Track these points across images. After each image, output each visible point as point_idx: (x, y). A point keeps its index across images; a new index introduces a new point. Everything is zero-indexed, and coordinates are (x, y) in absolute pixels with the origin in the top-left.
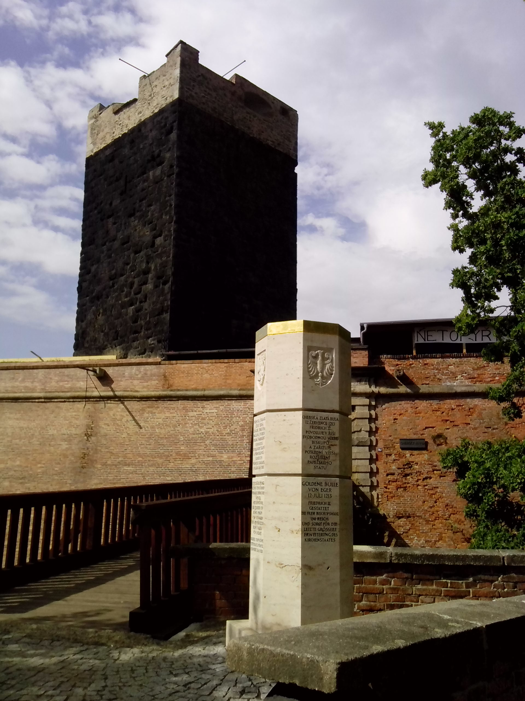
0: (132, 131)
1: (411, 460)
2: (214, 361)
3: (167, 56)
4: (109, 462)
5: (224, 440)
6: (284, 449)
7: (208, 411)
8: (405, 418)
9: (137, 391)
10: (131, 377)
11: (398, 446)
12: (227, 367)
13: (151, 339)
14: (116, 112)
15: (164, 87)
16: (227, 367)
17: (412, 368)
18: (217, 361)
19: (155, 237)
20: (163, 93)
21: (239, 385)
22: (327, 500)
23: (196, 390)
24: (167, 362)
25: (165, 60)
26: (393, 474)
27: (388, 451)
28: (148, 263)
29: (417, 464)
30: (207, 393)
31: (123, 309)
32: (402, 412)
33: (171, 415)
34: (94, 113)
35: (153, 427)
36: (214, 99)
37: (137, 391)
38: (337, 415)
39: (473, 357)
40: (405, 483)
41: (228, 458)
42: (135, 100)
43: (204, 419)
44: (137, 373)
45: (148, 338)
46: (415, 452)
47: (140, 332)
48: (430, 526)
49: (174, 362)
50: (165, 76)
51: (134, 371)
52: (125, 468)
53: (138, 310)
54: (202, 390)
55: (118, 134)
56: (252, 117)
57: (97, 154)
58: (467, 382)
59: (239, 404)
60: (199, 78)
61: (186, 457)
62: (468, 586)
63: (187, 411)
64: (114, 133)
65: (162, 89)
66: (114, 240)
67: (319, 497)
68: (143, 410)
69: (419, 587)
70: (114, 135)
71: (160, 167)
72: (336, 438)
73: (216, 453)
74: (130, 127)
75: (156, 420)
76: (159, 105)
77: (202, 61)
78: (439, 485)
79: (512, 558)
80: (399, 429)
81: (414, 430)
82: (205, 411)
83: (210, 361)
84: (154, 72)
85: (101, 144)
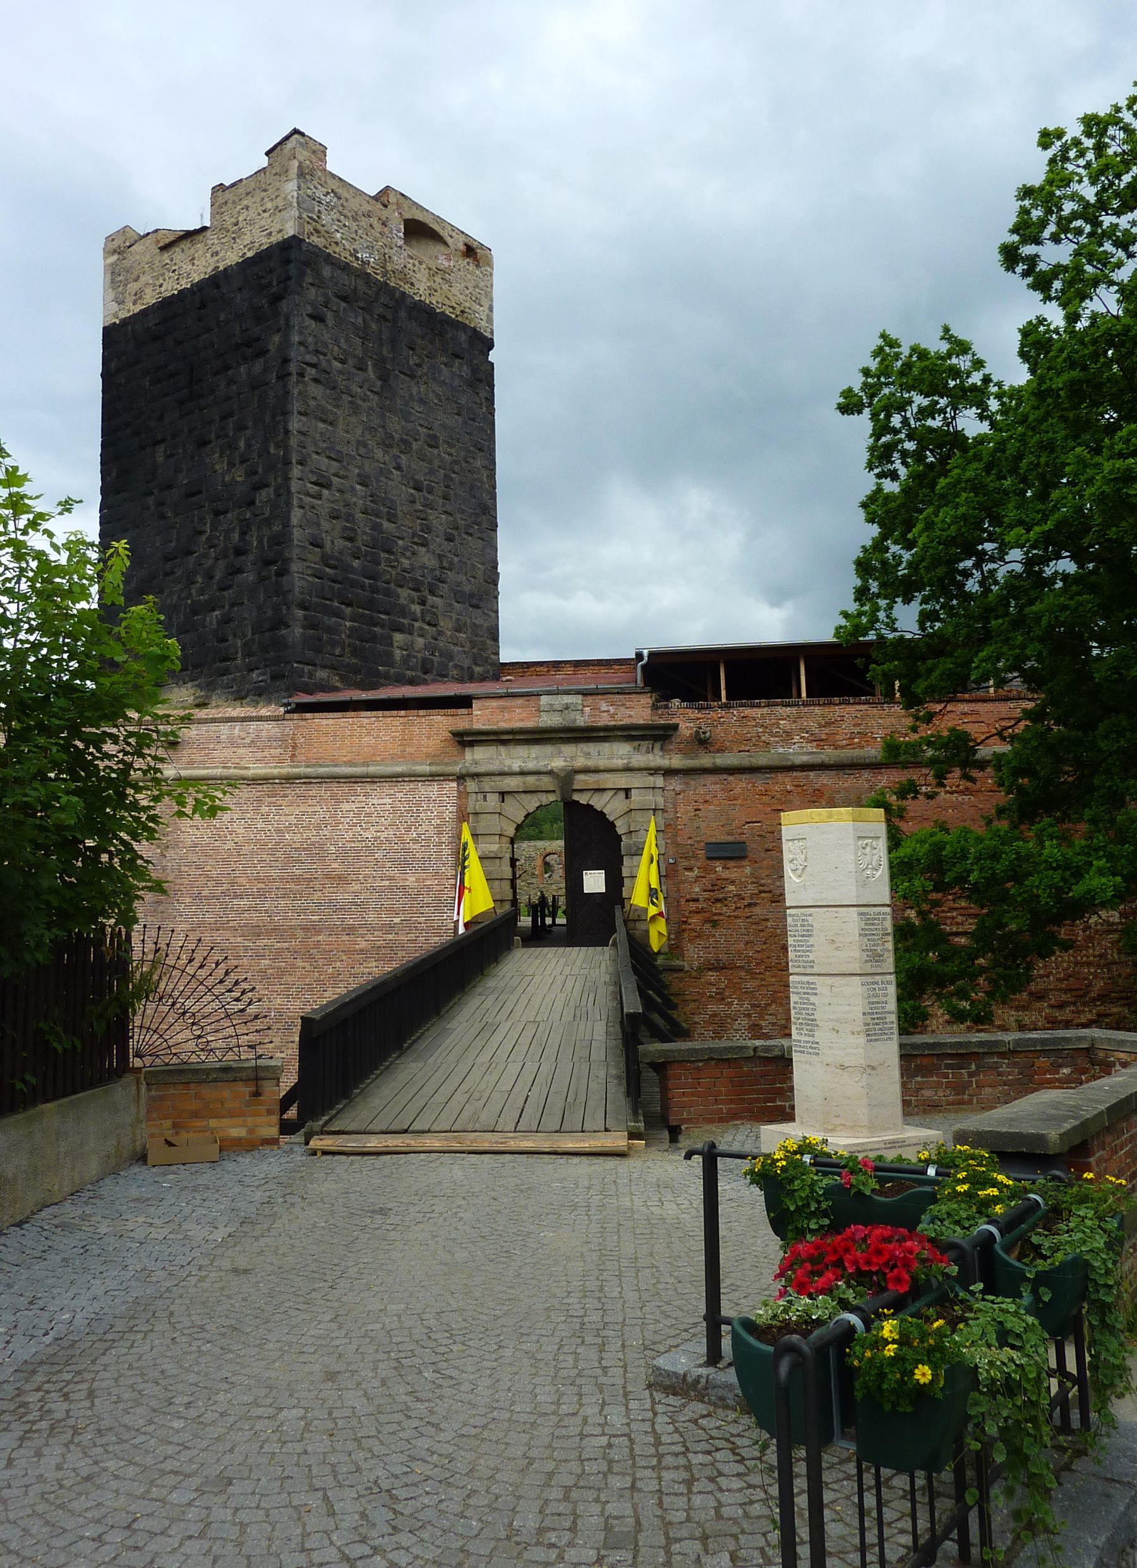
0: (198, 288)
1: (724, 876)
2: (380, 713)
3: (267, 154)
4: (204, 893)
5: (408, 851)
6: (837, 948)
7: (375, 802)
8: (712, 807)
9: (246, 768)
10: (233, 743)
11: (702, 854)
12: (404, 724)
13: (256, 672)
14: (165, 248)
15: (264, 211)
16: (404, 724)
17: (722, 724)
18: (388, 713)
19: (257, 488)
20: (263, 223)
21: (428, 756)
22: (884, 999)
23: (350, 764)
24: (296, 716)
25: (264, 162)
26: (697, 900)
27: (686, 863)
28: (243, 534)
29: (733, 882)
30: (372, 769)
31: (195, 615)
32: (708, 797)
33: (310, 809)
34: (116, 244)
35: (278, 831)
36: (354, 236)
37: (246, 768)
38: (888, 910)
39: (819, 705)
40: (716, 915)
41: (417, 880)
42: (204, 229)
43: (369, 815)
44: (243, 734)
45: (252, 670)
46: (731, 864)
47: (235, 659)
48: (758, 982)
49: (309, 715)
50: (265, 190)
51: (236, 731)
52: (235, 902)
53: (226, 620)
54: (363, 765)
55: (170, 288)
56: (417, 263)
57: (125, 322)
58: (811, 748)
59: (430, 788)
60: (328, 199)
61: (341, 880)
62: (971, 1075)
63: (339, 802)
64: (161, 286)
65: (259, 214)
66: (170, 487)
67: (877, 996)
68: (259, 800)
69: (919, 1079)
70: (163, 289)
71: (262, 360)
72: (888, 934)
73: (395, 872)
74: (196, 278)
75: (282, 818)
76: (257, 245)
77: (334, 164)
78: (770, 916)
79: (1017, 1042)
80: (703, 825)
81: (728, 828)
82: (371, 801)
83: (374, 713)
84: (241, 180)
85: (134, 304)
